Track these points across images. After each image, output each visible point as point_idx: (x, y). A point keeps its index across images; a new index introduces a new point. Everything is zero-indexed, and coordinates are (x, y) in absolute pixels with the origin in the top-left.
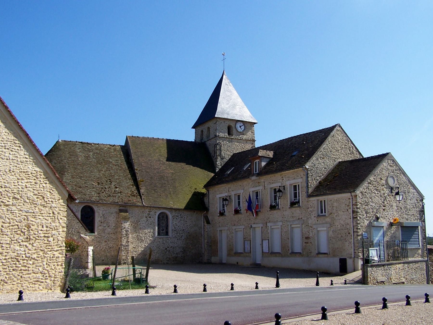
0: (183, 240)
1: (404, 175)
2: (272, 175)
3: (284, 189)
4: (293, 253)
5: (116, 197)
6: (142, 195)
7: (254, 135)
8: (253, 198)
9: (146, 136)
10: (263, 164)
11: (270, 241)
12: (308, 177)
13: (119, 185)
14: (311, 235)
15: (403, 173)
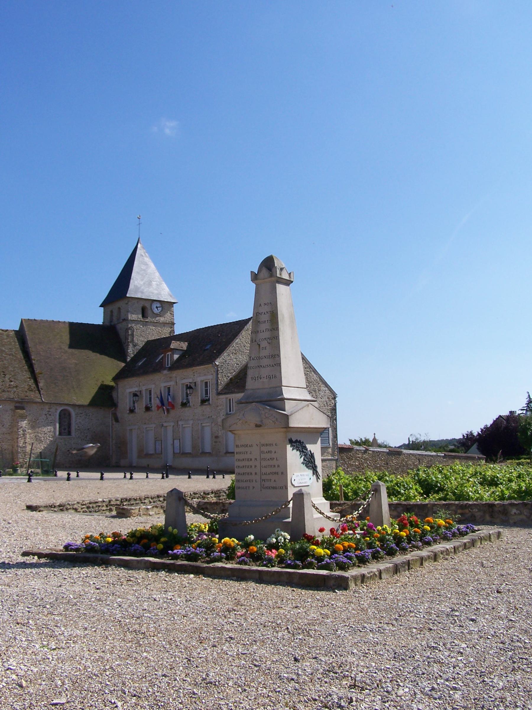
0: (88, 440)
1: (315, 373)
2: (184, 370)
3: (195, 385)
4: (204, 453)
5: (11, 392)
6: (40, 390)
7: (173, 316)
8: (165, 395)
9: (44, 319)
10: (176, 357)
11: (181, 440)
12: (218, 374)
13: (15, 379)
14: (220, 434)
15: (313, 371)
